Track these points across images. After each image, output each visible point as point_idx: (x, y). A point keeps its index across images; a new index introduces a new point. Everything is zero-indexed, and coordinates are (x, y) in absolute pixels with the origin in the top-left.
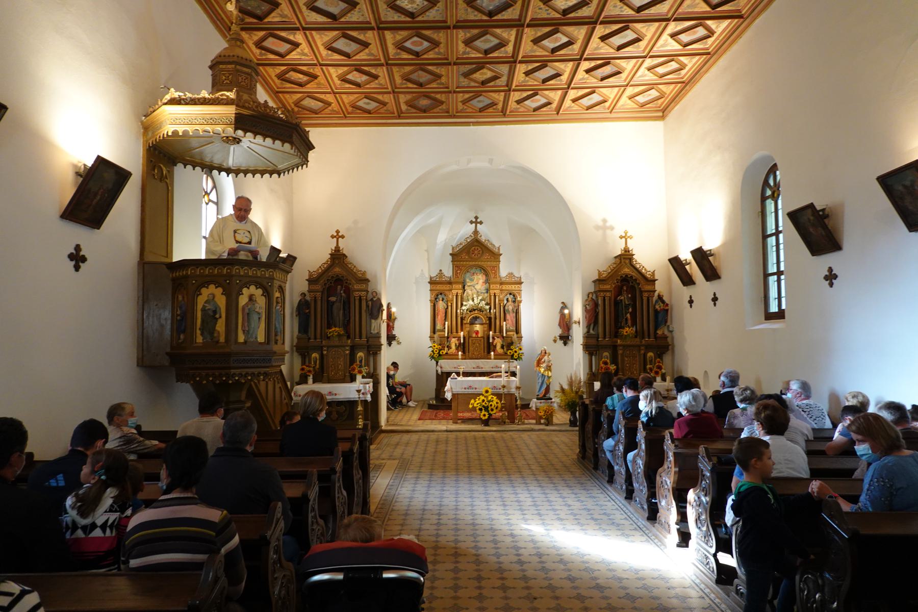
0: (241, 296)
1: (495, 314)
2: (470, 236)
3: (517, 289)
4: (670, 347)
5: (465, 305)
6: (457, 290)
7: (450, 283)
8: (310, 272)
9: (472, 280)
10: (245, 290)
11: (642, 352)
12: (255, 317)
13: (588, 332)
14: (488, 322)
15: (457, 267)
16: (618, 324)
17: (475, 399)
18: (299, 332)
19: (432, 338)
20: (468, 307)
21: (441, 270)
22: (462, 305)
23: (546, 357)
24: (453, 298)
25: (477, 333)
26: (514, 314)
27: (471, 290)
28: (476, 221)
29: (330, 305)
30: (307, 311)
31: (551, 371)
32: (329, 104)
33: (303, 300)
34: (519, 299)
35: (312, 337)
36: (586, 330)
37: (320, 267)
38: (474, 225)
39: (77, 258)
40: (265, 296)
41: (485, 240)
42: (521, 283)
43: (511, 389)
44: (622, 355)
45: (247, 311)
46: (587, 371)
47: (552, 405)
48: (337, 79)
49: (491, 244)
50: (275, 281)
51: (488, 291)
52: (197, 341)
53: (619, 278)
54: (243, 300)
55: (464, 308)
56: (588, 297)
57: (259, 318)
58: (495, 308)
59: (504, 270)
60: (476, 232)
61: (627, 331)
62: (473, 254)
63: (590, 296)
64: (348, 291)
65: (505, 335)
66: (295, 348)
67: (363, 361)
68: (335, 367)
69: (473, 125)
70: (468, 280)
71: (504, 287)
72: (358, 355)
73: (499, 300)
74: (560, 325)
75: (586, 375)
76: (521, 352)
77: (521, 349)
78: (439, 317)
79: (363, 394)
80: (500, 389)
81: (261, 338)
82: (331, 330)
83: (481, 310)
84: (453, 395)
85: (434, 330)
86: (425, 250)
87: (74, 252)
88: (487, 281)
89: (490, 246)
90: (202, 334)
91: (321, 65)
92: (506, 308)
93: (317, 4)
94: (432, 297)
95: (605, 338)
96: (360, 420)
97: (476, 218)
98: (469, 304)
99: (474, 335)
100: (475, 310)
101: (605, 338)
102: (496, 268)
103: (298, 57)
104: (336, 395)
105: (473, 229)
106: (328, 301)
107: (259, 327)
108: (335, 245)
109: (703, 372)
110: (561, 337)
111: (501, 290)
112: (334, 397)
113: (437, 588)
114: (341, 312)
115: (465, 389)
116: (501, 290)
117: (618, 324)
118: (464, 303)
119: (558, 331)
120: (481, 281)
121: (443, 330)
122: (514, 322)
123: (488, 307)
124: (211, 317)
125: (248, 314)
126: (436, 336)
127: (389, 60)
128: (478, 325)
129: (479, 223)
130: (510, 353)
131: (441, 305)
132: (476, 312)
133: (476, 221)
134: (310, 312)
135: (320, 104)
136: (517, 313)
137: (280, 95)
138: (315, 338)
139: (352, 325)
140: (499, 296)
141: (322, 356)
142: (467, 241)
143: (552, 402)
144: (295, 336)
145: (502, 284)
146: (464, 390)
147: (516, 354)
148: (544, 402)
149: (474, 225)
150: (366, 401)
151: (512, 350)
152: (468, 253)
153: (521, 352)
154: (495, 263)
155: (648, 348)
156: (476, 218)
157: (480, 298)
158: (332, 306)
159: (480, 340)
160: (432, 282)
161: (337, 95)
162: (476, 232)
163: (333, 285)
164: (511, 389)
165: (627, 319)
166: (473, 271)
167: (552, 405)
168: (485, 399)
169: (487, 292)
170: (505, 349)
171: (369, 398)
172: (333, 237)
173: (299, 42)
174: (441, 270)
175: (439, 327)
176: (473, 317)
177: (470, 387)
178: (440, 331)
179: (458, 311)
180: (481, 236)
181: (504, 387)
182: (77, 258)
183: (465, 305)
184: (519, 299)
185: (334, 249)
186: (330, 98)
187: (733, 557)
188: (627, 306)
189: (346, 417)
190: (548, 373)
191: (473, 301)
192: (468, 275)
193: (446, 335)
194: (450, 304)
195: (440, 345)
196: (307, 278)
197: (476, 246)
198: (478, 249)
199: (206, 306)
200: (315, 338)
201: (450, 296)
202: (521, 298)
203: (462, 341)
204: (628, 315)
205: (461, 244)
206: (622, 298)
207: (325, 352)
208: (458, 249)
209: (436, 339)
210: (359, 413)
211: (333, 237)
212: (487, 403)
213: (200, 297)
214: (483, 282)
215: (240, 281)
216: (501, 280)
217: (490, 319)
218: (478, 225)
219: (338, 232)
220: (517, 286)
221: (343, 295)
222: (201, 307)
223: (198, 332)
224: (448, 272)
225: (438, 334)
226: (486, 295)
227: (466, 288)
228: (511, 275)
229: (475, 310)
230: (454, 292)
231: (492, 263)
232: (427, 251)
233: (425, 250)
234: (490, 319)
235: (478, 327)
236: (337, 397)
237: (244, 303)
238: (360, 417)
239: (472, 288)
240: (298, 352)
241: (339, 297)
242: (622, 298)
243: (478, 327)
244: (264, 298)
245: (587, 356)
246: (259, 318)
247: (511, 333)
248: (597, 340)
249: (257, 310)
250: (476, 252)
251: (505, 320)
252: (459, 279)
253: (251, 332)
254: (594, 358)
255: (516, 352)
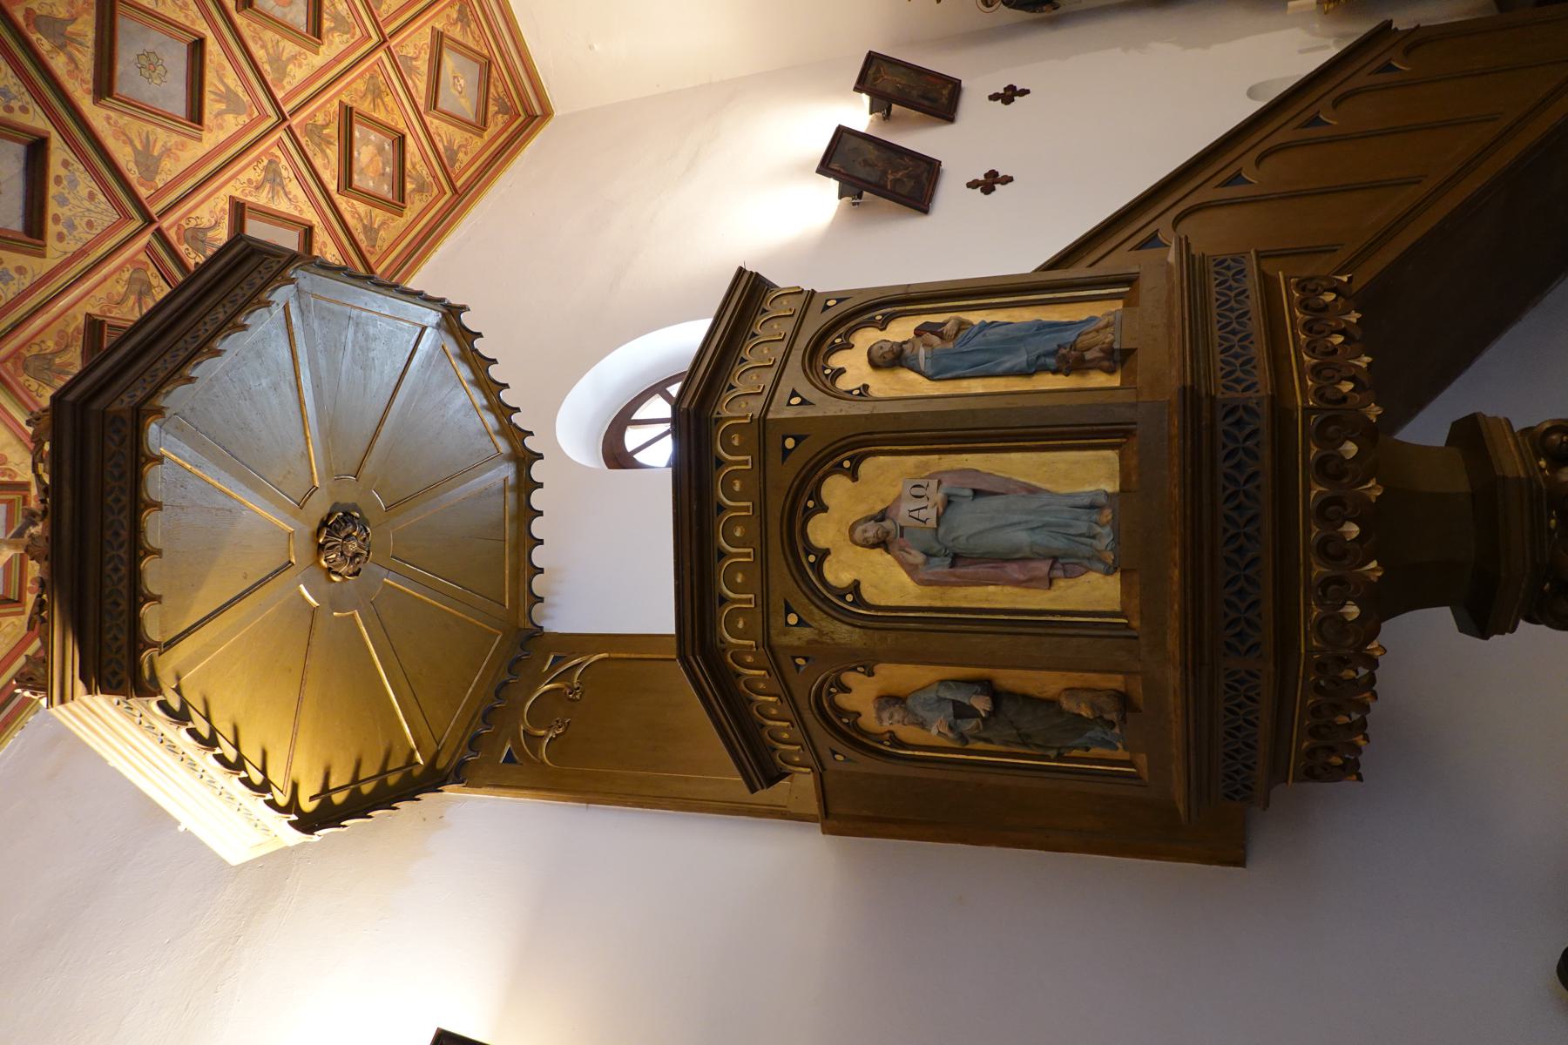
0: (868, 594)
10: (838, 573)
32: (439, 38)
39: (990, 182)
40: (857, 461)
45: (941, 567)
48: (322, 49)
50: (782, 411)
57: (977, 493)
87: (979, 188)
91: (283, 118)
93: (16, 224)
103: (294, 188)
107: (1033, 491)
135: (450, 62)
137: (458, 184)
161: (387, 31)
173: (227, 207)
182: (990, 182)
186: (415, 44)
187: (720, 595)
237: (903, 577)
244: (867, 467)
246: (977, 493)
249: (930, 514)
253: (1059, 544)
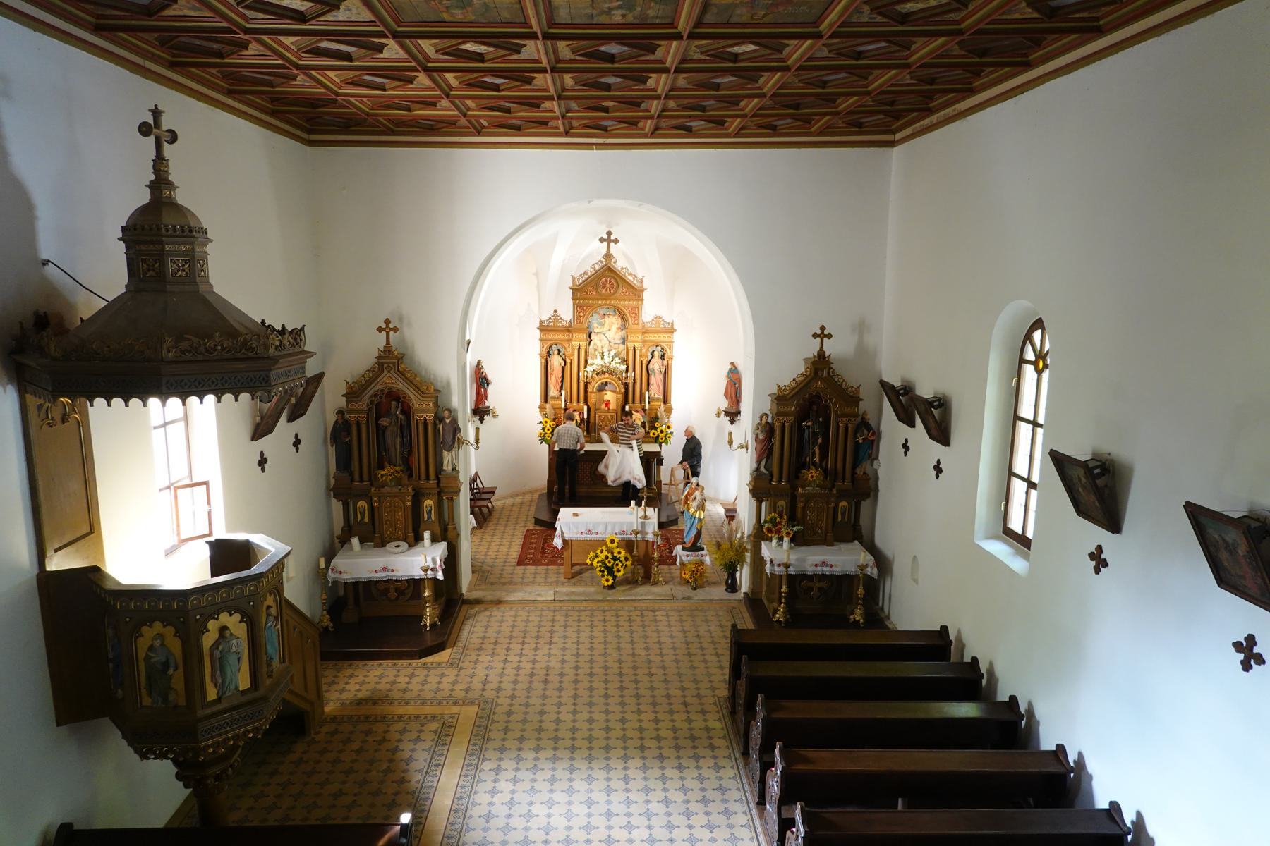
1: (634, 380)
2: (600, 261)
3: (667, 339)
4: (872, 494)
5: (591, 365)
6: (579, 340)
7: (568, 329)
8: (347, 383)
9: (602, 325)
11: (832, 505)
12: (232, 659)
13: (758, 469)
14: (623, 390)
15: (580, 307)
16: (799, 465)
17: (594, 552)
18: (337, 469)
19: (542, 408)
20: (595, 367)
21: (556, 311)
22: (586, 362)
23: (697, 493)
24: (573, 352)
25: (607, 403)
26: (662, 376)
27: (600, 340)
28: (609, 239)
29: (381, 431)
30: (347, 439)
31: (704, 511)
33: (340, 422)
34: (669, 354)
35: (357, 476)
36: (755, 466)
37: (363, 376)
38: (605, 243)
41: (622, 268)
42: (672, 331)
43: (647, 534)
44: (803, 508)
46: (754, 521)
47: (703, 558)
49: (631, 274)
51: (624, 341)
52: (144, 704)
53: (807, 396)
54: (209, 639)
55: (589, 369)
56: (761, 420)
57: (239, 659)
58: (634, 370)
59: (650, 309)
60: (608, 256)
61: (812, 475)
62: (604, 288)
63: (764, 419)
64: (407, 411)
65: (647, 407)
66: (332, 493)
67: (433, 512)
68: (391, 524)
69: (597, 149)
70: (595, 325)
71: (648, 337)
72: (425, 504)
73: (641, 356)
74: (726, 395)
75: (752, 529)
76: (669, 431)
77: (669, 427)
78: (553, 378)
79: (432, 570)
80: (631, 534)
81: (244, 682)
82: (383, 473)
83: (612, 373)
84: (565, 542)
85: (545, 397)
86: (534, 274)
88: (624, 326)
89: (629, 277)
90: (150, 694)
92: (650, 366)
94: (541, 350)
95: (780, 481)
96: (428, 610)
97: (609, 233)
98: (596, 363)
99: (603, 406)
100: (604, 373)
101: (780, 481)
102: (636, 311)
104: (393, 571)
105: (604, 251)
106: (378, 426)
108: (384, 343)
109: (912, 556)
110: (727, 413)
111: (644, 341)
112: (390, 573)
113: (555, 713)
114: (398, 440)
115: (582, 533)
116: (644, 341)
117: (799, 465)
118: (590, 361)
119: (724, 404)
120: (615, 327)
121: (559, 398)
122: (661, 387)
123: (623, 367)
124: (159, 673)
125: (219, 658)
126: (548, 406)
127: (451, 90)
128: (608, 393)
129: (613, 241)
130: (654, 434)
131: (556, 361)
132: (607, 375)
133: (609, 239)
134: (351, 441)
136: (666, 374)
138: (361, 479)
139: (414, 458)
140: (641, 350)
141: (372, 508)
142: (594, 268)
143: (703, 555)
144: (332, 475)
145: (646, 332)
146: (579, 535)
147: (662, 435)
148: (692, 556)
149: (605, 244)
150: (435, 580)
151: (656, 428)
152: (595, 287)
153: (669, 431)
154: (635, 303)
155: (842, 495)
156: (609, 233)
157: (612, 353)
158: (384, 432)
159: (612, 416)
160: (543, 328)
162: (608, 256)
163: (383, 400)
164: (647, 534)
165: (814, 453)
166: (603, 311)
167: (703, 558)
168: (610, 555)
169: (623, 343)
170: (647, 429)
171: (440, 576)
172: (380, 330)
174: (556, 311)
175: (553, 392)
176: (602, 383)
177: (589, 531)
178: (553, 398)
179: (581, 374)
180: (615, 262)
181: (636, 533)
183: (591, 365)
184: (669, 354)
185: (382, 349)
188: (815, 435)
189: (410, 595)
190: (700, 515)
191: (602, 358)
192: (596, 316)
193: (563, 406)
194: (568, 361)
195: (554, 420)
196: (345, 392)
197: (609, 276)
198: (606, 281)
199: (151, 658)
200: (361, 479)
201: (569, 349)
202: (672, 352)
203: (586, 417)
204: (817, 449)
205: (585, 273)
206: (809, 424)
207: (376, 504)
208: (581, 281)
209: (548, 411)
210: (427, 599)
211: (380, 330)
212: (612, 561)
213: (141, 639)
214: (618, 328)
215: (201, 615)
216: (644, 326)
217: (626, 385)
218: (612, 244)
219: (387, 322)
220: (666, 335)
221: (400, 416)
222: (144, 655)
223: (144, 692)
224: (567, 313)
225: (551, 402)
226: (622, 347)
227: (593, 336)
228: (658, 319)
229: (604, 373)
230: (576, 344)
231: (631, 302)
232: (536, 274)
233: (534, 274)
234: (626, 385)
235: (609, 396)
236: (395, 574)
238: (428, 604)
239: (603, 336)
240: (336, 498)
241: (394, 417)
242: (809, 424)
243: (609, 396)
245: (754, 503)
246: (239, 659)
247: (656, 403)
248: (770, 483)
250: (608, 285)
251: (648, 390)
252: (581, 326)
254: (764, 504)
255: (662, 432)
